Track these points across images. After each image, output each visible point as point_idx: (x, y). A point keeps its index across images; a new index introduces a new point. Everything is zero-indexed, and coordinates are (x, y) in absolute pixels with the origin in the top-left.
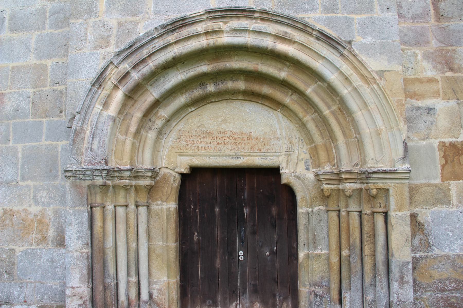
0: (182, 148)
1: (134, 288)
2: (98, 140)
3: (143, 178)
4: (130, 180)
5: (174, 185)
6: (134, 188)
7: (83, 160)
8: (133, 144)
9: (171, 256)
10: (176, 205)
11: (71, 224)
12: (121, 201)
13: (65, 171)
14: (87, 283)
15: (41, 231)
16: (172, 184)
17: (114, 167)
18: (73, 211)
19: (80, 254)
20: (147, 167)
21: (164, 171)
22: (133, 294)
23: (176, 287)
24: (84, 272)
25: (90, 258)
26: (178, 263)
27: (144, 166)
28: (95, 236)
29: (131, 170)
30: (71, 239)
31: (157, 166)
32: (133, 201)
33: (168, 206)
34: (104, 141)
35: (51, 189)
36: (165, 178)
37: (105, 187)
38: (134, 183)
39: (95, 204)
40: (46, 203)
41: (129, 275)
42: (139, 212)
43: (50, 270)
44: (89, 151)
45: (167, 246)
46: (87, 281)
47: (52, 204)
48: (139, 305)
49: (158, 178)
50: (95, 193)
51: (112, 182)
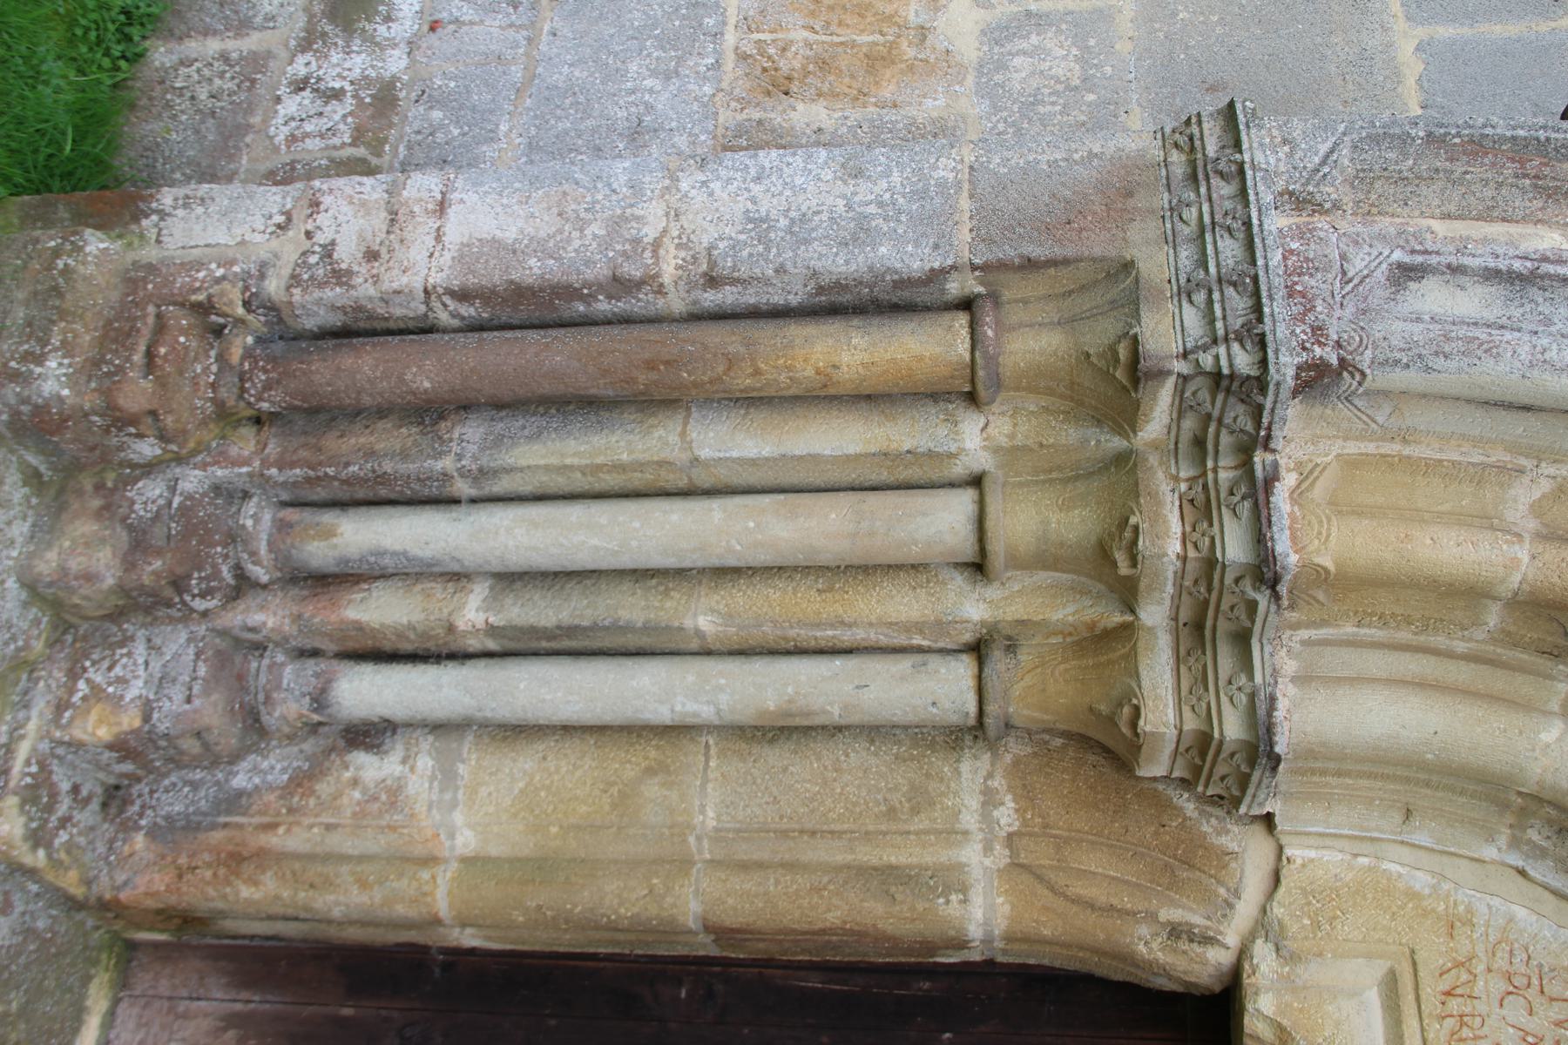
0: (1454, 1005)
1: (417, 617)
2: (1489, 315)
3: (1196, 681)
4: (1181, 575)
5: (1144, 930)
6: (1118, 618)
7: (1321, 222)
8: (1468, 594)
9: (611, 886)
10: (988, 941)
11: (858, 174)
12: (1021, 520)
13: (1230, 111)
14: (456, 284)
15: (824, 65)
16: (1152, 917)
17: (1276, 443)
18: (942, 184)
19: (650, 233)
20: (1282, 705)
21: (1254, 853)
22: (382, 610)
23: (401, 910)
24: (533, 262)
25: (620, 306)
26: (566, 941)
27: (1292, 690)
28: (767, 334)
29: (1265, 571)
30: (758, 179)
31: (1288, 797)
32: (1015, 611)
33: (978, 875)
34: (1491, 350)
35: (1091, 97)
36: (1191, 864)
37: (1119, 381)
38: (1155, 614)
39: (998, 323)
40: (998, 78)
41: (510, 579)
42: (934, 661)
43: (589, 123)
44: (1398, 255)
45: (684, 864)
46: (472, 280)
47: (996, 109)
48: (315, 653)
49: (1190, 808)
50: (1073, 320)
51: (1155, 445)
